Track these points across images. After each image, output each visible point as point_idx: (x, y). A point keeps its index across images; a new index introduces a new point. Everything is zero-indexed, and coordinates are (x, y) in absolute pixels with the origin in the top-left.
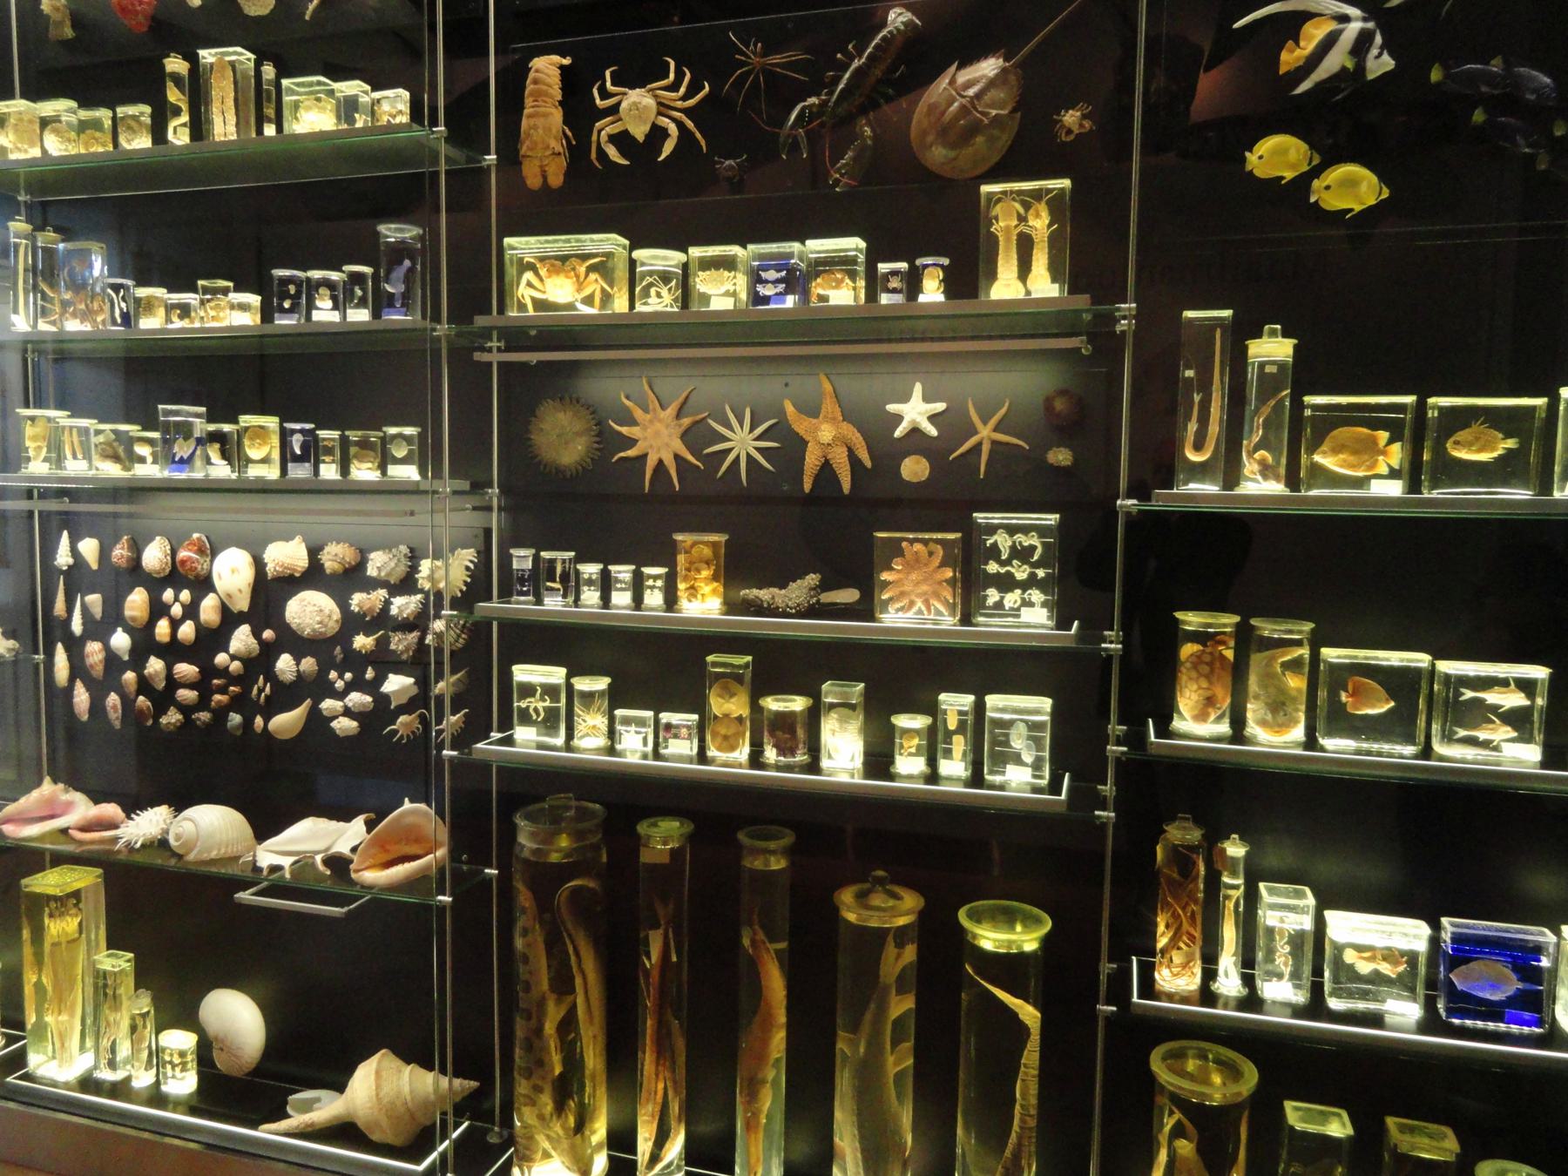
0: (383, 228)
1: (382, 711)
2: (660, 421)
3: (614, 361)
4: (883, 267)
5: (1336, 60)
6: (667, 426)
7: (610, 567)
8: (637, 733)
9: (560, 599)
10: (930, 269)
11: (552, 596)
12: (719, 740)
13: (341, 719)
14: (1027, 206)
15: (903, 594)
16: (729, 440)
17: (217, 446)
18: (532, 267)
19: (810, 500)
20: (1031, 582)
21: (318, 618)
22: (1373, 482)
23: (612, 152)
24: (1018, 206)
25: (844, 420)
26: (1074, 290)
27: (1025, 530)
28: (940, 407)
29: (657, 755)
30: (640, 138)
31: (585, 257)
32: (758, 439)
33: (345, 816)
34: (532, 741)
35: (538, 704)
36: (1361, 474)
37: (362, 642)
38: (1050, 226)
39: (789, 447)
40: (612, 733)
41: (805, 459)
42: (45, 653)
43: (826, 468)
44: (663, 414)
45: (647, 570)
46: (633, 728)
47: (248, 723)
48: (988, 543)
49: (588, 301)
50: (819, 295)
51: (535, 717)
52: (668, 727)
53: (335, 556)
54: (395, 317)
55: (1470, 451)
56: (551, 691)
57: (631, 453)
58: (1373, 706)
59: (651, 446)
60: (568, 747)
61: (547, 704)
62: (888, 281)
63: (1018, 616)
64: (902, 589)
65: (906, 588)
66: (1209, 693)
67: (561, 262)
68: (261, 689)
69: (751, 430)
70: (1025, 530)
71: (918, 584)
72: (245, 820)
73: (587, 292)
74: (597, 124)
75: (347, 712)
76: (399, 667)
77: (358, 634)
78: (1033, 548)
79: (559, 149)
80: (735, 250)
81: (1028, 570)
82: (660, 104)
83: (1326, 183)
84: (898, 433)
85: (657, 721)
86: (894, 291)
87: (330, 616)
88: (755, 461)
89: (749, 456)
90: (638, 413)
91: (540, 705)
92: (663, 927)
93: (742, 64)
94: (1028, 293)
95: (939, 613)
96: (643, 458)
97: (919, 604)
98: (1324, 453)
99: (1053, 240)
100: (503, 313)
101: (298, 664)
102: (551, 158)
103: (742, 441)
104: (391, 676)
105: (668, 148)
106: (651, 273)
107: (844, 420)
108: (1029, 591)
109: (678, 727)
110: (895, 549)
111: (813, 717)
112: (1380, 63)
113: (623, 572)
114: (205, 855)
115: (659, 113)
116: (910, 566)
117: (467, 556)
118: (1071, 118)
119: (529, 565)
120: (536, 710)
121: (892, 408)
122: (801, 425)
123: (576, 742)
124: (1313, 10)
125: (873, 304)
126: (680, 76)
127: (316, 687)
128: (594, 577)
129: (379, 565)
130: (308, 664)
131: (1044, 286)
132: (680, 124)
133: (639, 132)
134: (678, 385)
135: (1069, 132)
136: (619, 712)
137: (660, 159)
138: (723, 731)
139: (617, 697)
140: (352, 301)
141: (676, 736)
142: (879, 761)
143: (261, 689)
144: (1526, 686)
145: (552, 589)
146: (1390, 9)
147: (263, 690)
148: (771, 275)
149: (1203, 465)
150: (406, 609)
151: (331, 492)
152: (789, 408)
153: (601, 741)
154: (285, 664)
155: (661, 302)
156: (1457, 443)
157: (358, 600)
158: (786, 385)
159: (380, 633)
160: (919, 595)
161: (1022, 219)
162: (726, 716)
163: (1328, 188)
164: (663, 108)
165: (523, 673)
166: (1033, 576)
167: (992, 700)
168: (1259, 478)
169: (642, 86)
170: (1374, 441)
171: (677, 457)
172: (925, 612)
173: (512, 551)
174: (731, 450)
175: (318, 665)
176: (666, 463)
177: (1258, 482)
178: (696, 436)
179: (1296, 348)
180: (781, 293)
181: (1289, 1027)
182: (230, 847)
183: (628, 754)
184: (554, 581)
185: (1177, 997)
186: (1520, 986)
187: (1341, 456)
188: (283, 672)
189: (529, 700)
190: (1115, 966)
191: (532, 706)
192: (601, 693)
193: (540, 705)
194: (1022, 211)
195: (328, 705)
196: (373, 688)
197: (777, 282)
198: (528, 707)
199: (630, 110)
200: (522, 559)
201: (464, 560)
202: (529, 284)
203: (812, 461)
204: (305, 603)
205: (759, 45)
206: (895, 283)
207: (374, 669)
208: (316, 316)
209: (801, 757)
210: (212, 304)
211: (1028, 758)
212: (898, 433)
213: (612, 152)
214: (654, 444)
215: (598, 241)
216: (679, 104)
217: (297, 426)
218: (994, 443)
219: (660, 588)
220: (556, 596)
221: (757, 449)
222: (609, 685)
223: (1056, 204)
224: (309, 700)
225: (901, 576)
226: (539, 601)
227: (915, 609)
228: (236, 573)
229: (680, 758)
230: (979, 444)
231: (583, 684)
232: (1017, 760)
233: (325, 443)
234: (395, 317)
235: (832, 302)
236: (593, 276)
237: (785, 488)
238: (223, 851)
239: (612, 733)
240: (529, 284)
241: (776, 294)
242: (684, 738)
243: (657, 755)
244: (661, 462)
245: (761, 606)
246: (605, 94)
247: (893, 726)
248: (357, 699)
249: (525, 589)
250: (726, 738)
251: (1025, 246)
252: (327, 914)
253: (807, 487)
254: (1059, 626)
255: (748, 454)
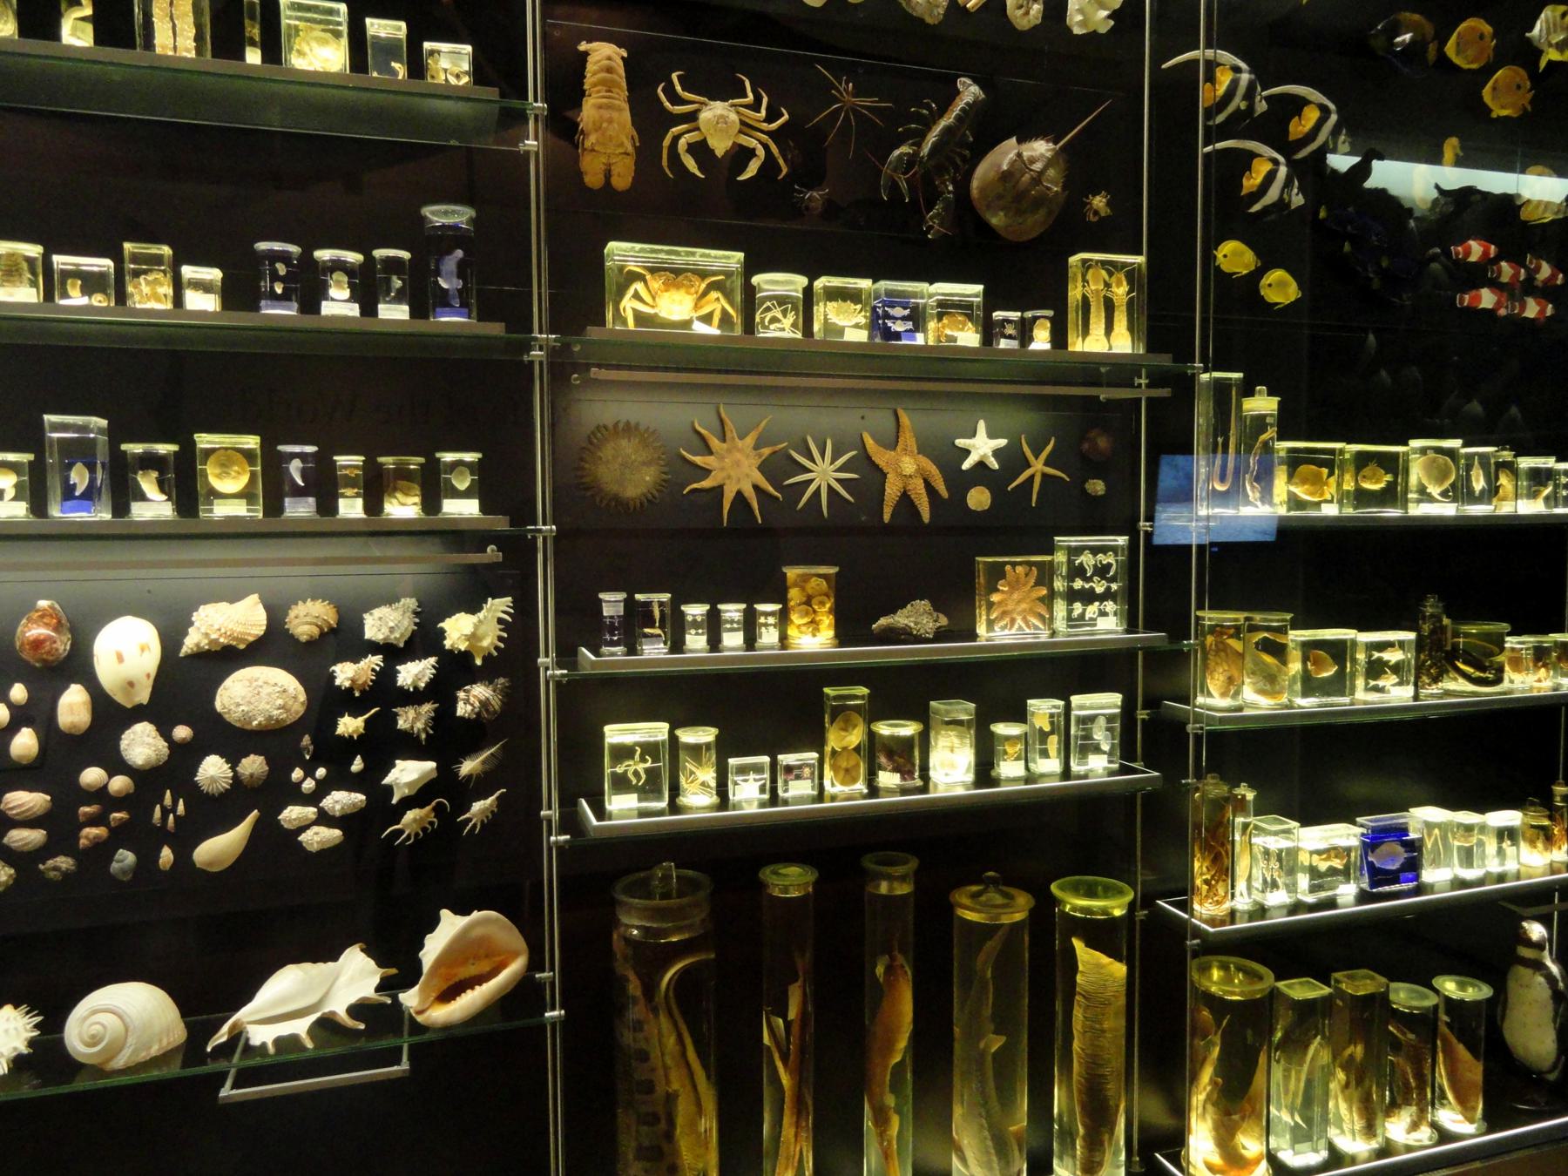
0: (427, 211)
1: (382, 809)
2: (739, 450)
3: (613, 382)
4: (998, 315)
5: (1273, 195)
6: (748, 456)
7: (720, 607)
8: (755, 780)
9: (662, 645)
10: (1042, 320)
11: (653, 644)
12: (842, 773)
13: (315, 829)
14: (1111, 274)
15: (1004, 614)
16: (810, 471)
17: (155, 474)
18: (641, 278)
19: (732, 532)
20: (1107, 595)
21: (280, 702)
22: (1323, 505)
23: (691, 164)
24: (1104, 273)
25: (919, 453)
26: (1151, 348)
27: (1103, 550)
28: (1002, 442)
29: (774, 800)
30: (719, 153)
31: (703, 274)
32: (839, 470)
33: (328, 952)
34: (630, 810)
35: (636, 767)
36: (1316, 499)
37: (349, 725)
38: (1128, 293)
39: (869, 477)
40: (722, 789)
41: (884, 490)
42: (1135, 720)
43: (905, 499)
44: (740, 444)
45: (761, 607)
46: (752, 776)
47: (147, 858)
48: (1077, 562)
49: (707, 319)
50: (947, 336)
51: (634, 782)
52: (789, 769)
53: (308, 618)
54: (450, 319)
55: (1371, 483)
56: (650, 749)
57: (706, 484)
58: (1327, 671)
59: (729, 477)
60: (674, 808)
61: (648, 765)
62: (1004, 327)
63: (1095, 625)
64: (1005, 609)
65: (1010, 608)
66: (1228, 674)
67: (675, 275)
68: (170, 808)
69: (832, 463)
70: (1103, 550)
71: (1019, 602)
72: (167, 996)
73: (705, 311)
74: (674, 130)
75: (324, 819)
76: (411, 747)
77: (343, 716)
78: (1110, 565)
79: (630, 149)
80: (865, 284)
81: (1106, 584)
82: (742, 123)
83: (1268, 282)
84: (966, 466)
85: (774, 764)
86: (1010, 337)
87: (295, 698)
88: (837, 494)
89: (830, 487)
90: (715, 443)
91: (641, 767)
92: (801, 979)
93: (837, 100)
94: (1110, 348)
95: (1036, 628)
96: (718, 491)
97: (1019, 621)
98: (1296, 484)
99: (1130, 304)
100: (991, 345)
101: (233, 768)
102: (620, 157)
103: (825, 472)
104: (397, 762)
105: (752, 169)
106: (770, 298)
107: (919, 453)
108: (1105, 603)
109: (800, 767)
110: (997, 573)
111: (924, 739)
112: (1298, 200)
113: (732, 611)
114: (143, 1054)
115: (740, 132)
116: (1014, 587)
117: (498, 607)
118: (1099, 202)
119: (621, 610)
120: (636, 773)
121: (960, 442)
122: (881, 457)
123: (684, 800)
124: (1257, 152)
125: (371, 319)
126: (758, 99)
127: (277, 791)
128: (699, 619)
129: (392, 624)
130: (253, 765)
131: (1122, 343)
132: (766, 147)
133: (720, 146)
134: (770, 416)
135: (1096, 213)
136: (732, 761)
137: (780, 178)
138: (844, 765)
139: (725, 748)
140: (388, 294)
141: (798, 777)
142: (984, 771)
143: (170, 808)
144: (1402, 645)
145: (652, 636)
146: (1295, 160)
147: (174, 810)
148: (898, 312)
149: (1226, 492)
150: (424, 676)
151: (304, 535)
152: (869, 442)
153: (711, 799)
154: (213, 770)
155: (781, 328)
156: (1364, 477)
157: (345, 673)
158: (863, 418)
159: (373, 711)
160: (1019, 614)
161: (1107, 285)
162: (845, 749)
163: (1270, 285)
164: (746, 127)
165: (616, 734)
166: (1109, 588)
167: (1076, 700)
168: (1259, 503)
169: (724, 100)
170: (1319, 475)
171: (756, 488)
172: (1025, 628)
173: (602, 596)
174: (812, 481)
175: (268, 764)
176: (746, 495)
177: (1257, 507)
178: (778, 467)
179: (1279, 403)
180: (910, 331)
181: (1250, 928)
182: (171, 1034)
183: (744, 804)
184: (653, 626)
185: (1218, 922)
186: (1406, 855)
187: (1306, 487)
188: (213, 780)
189: (627, 763)
190: (1146, 912)
191: (631, 770)
192: (708, 746)
193: (641, 767)
194: (1107, 277)
195: (293, 814)
196: (371, 782)
197: (904, 319)
198: (626, 771)
199: (718, 123)
200: (612, 603)
201: (496, 611)
202: (637, 296)
203: (892, 491)
204: (260, 683)
205: (851, 85)
206: (1010, 330)
207: (364, 760)
208: (327, 308)
209: (919, 783)
210: (150, 277)
211: (1106, 747)
212: (966, 466)
213: (691, 164)
214: (732, 474)
215: (715, 257)
216: (765, 126)
217: (297, 449)
218: (1044, 475)
219: (775, 626)
220: (659, 644)
221: (838, 480)
222: (717, 737)
223: (1132, 275)
224: (256, 811)
225: (1005, 596)
226: (632, 650)
227: (1016, 626)
228: (146, 653)
229: (800, 800)
230: (1032, 477)
231: (688, 736)
232: (1097, 749)
233: (344, 472)
234: (450, 319)
235: (960, 343)
236: (714, 295)
237: (863, 519)
238: (165, 1042)
239: (722, 789)
240: (637, 296)
241: (906, 331)
242: (807, 778)
243: (774, 800)
244: (739, 494)
245: (911, 634)
246: (676, 100)
247: (992, 734)
248: (340, 800)
249: (616, 638)
250: (847, 771)
251: (1109, 307)
252: (289, 1092)
253: (887, 518)
254: (1128, 631)
255: (829, 486)
